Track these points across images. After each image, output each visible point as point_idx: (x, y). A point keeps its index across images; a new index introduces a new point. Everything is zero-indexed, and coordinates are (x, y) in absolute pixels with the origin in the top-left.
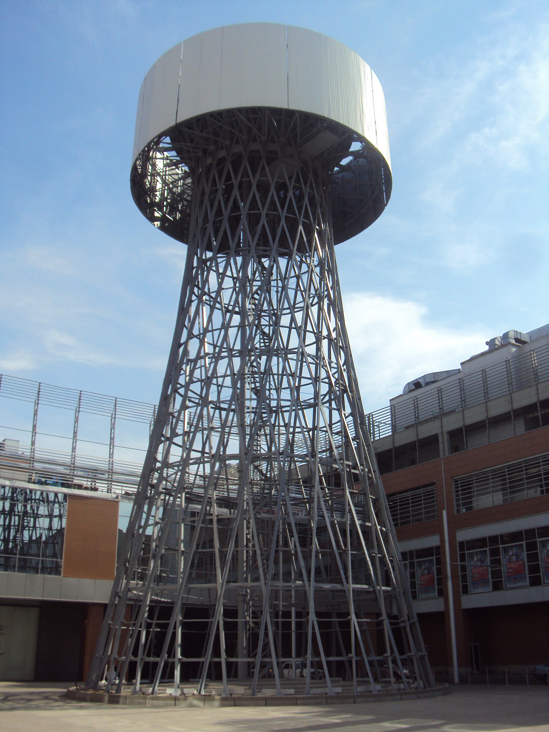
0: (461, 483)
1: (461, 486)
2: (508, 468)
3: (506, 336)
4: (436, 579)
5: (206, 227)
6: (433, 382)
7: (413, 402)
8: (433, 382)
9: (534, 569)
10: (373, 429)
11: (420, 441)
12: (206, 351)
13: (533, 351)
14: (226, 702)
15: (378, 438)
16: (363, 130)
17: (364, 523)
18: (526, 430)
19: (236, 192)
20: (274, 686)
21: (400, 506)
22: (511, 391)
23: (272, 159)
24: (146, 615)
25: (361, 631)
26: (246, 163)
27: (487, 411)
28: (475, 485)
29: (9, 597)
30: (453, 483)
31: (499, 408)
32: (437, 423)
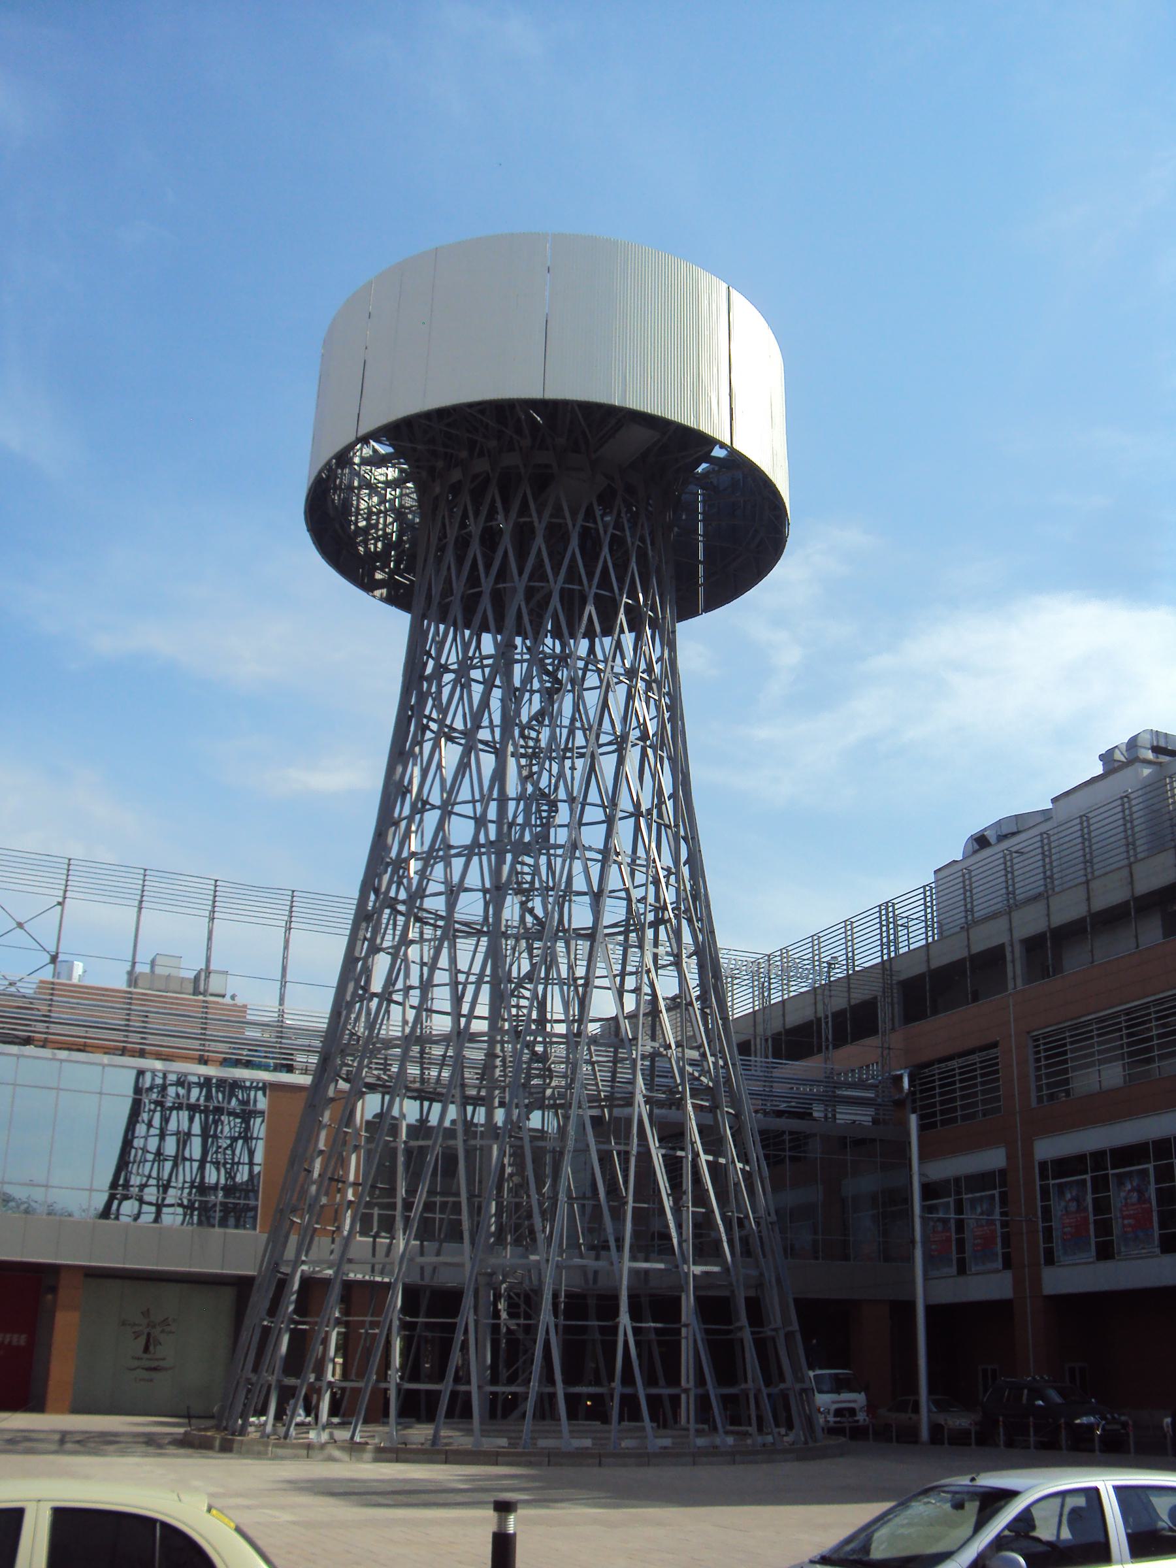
0: (1044, 1044)
1: (1046, 1050)
2: (1127, 1014)
3: (1133, 743)
4: (999, 1234)
5: (449, 603)
6: (1013, 834)
7: (961, 879)
8: (1013, 834)
9: (1104, 1227)
10: (895, 933)
11: (973, 958)
12: (413, 849)
13: (1171, 777)
14: (383, 1455)
15: (906, 949)
16: (697, 417)
17: (671, 1152)
18: (1166, 935)
19: (475, 548)
20: (469, 1432)
21: (961, 1081)
22: (1132, 859)
23: (543, 482)
24: (291, 1308)
25: (637, 1343)
26: (493, 491)
27: (1088, 899)
28: (1154, 1032)
29: (127, 1266)
30: (1031, 1044)
31: (1109, 894)
32: (1002, 922)
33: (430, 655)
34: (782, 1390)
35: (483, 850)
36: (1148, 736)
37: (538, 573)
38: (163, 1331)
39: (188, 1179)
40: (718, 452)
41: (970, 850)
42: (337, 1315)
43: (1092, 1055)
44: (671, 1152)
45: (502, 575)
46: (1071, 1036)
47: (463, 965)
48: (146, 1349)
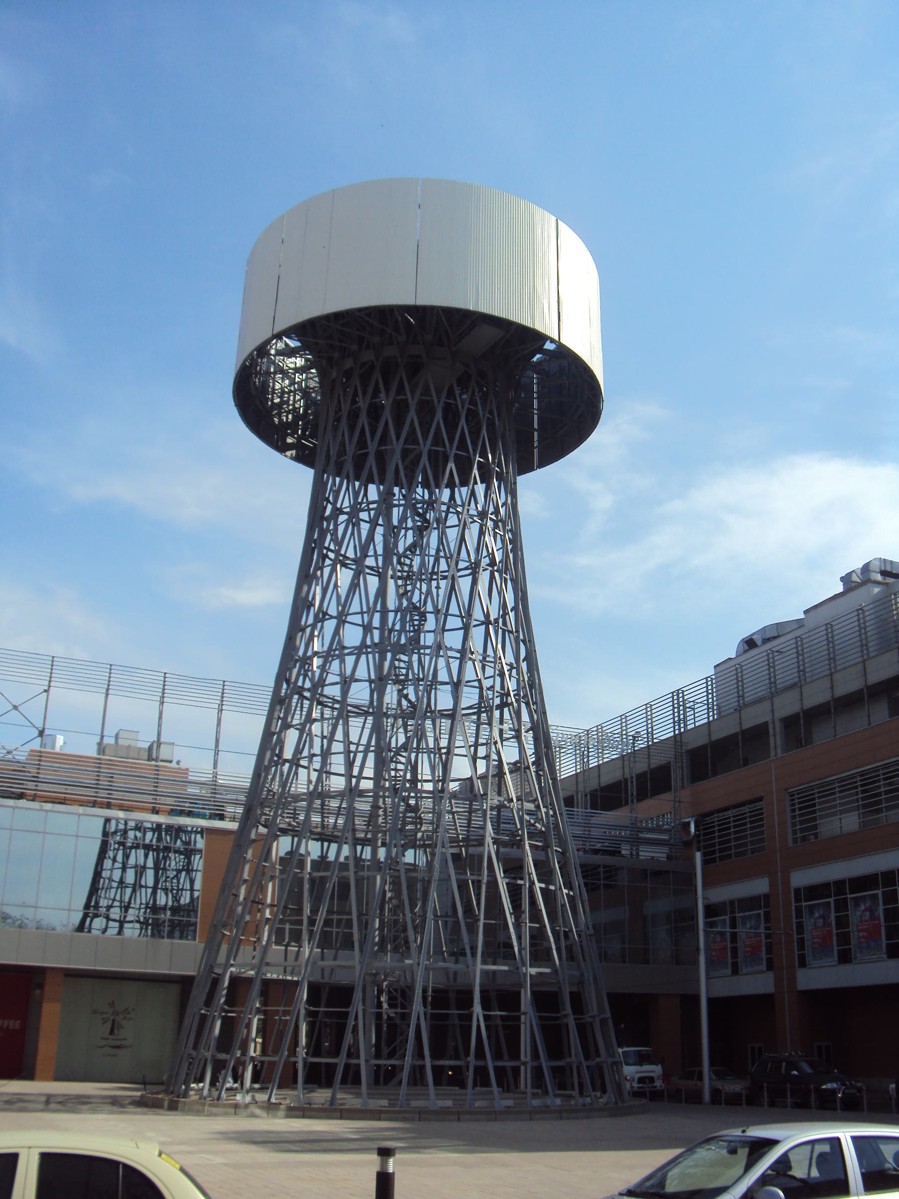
0: (798, 798)
1: (800, 803)
2: (862, 776)
3: (866, 568)
4: (764, 944)
5: (343, 461)
6: (775, 638)
7: (734, 672)
8: (775, 638)
9: (844, 939)
10: (684, 714)
11: (744, 732)
12: (316, 649)
13: (895, 594)
14: (293, 1113)
15: (693, 726)
16: (533, 319)
17: (513, 881)
18: (891, 715)
19: (363, 419)
20: (359, 1095)
21: (735, 827)
22: (865, 657)
23: (415, 369)
24: (223, 1000)
25: (487, 1027)
26: (377, 376)
27: (832, 688)
28: (882, 790)
29: (97, 968)
30: (788, 798)
31: (848, 684)
32: (766, 705)
33: (328, 501)
34: (597, 1063)
35: (369, 650)
36: (878, 563)
37: (412, 438)
38: (124, 1018)
39: (144, 901)
40: (549, 346)
41: (742, 650)
42: (258, 1005)
43: (835, 806)
44: (513, 881)
45: (384, 440)
46: (819, 792)
47: (354, 738)
48: (112, 1032)
